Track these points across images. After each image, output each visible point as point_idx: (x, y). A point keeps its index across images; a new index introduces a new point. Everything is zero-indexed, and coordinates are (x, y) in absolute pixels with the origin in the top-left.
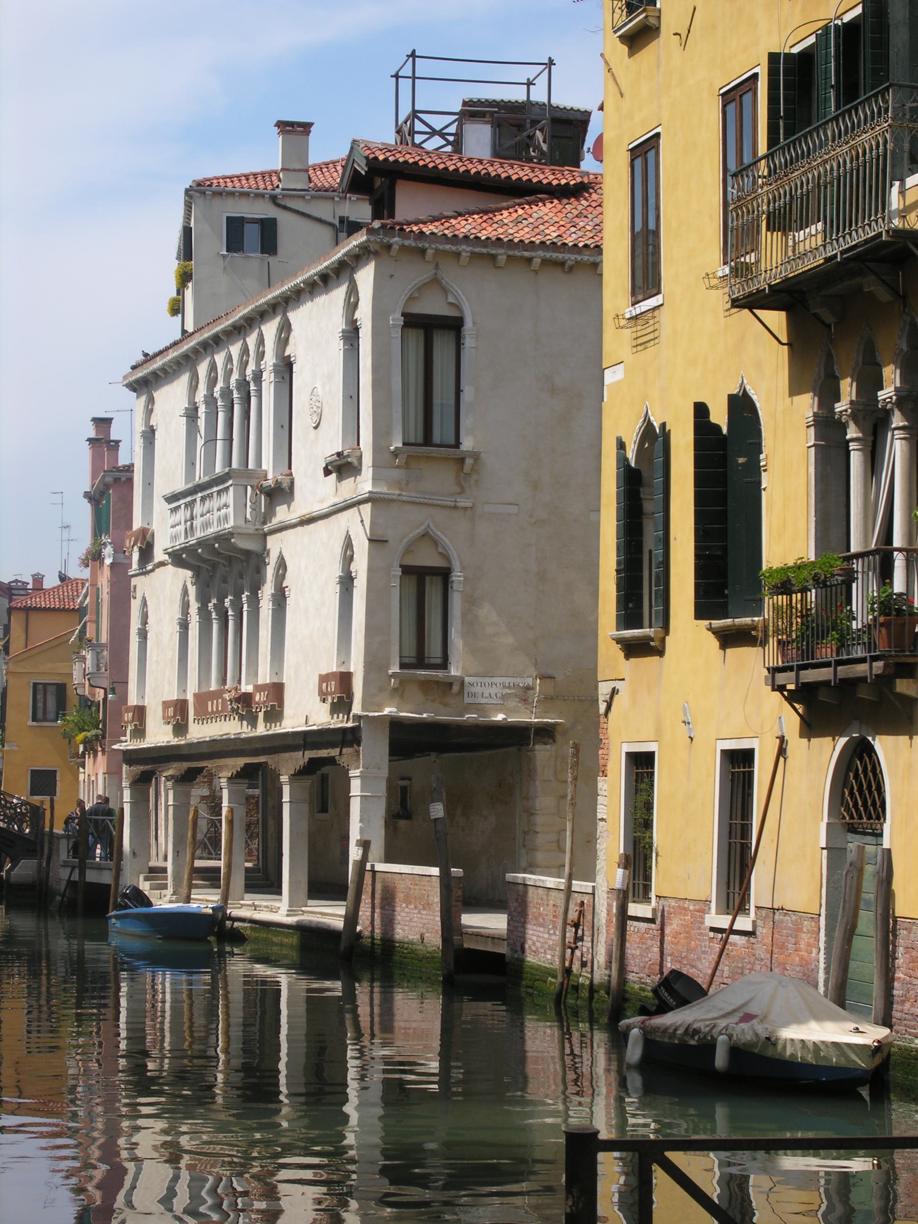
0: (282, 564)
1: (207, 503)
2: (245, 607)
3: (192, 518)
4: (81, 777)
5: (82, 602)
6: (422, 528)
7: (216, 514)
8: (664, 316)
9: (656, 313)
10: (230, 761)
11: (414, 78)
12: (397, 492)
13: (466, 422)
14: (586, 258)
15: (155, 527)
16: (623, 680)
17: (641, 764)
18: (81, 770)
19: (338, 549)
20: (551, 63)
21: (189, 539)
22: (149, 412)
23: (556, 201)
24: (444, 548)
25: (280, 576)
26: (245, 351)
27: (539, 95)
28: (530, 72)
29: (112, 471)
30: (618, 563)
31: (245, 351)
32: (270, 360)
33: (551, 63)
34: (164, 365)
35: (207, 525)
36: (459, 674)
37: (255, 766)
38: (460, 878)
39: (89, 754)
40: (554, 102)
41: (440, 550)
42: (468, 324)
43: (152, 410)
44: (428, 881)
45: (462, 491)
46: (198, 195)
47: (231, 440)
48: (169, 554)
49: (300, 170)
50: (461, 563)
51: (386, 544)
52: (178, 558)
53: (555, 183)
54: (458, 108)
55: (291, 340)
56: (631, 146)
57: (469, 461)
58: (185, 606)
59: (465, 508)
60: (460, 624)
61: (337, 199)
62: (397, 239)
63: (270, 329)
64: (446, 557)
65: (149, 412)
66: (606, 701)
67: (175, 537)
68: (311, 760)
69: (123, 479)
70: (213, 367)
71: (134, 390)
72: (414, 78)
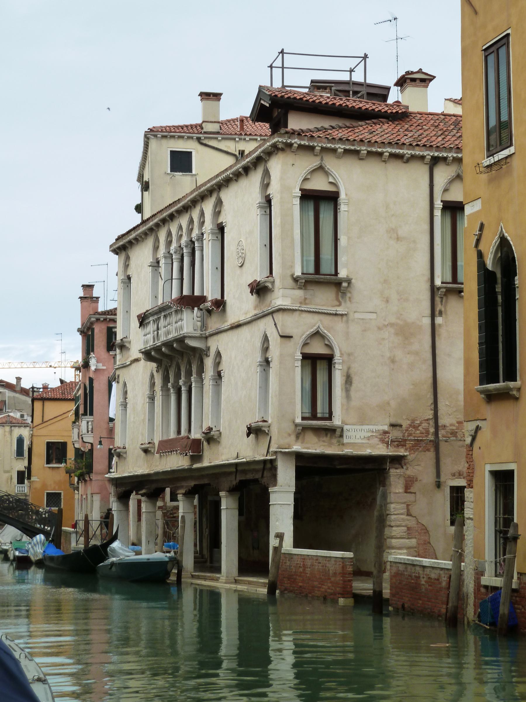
0: (218, 354)
1: (168, 319)
2: (193, 385)
3: (158, 329)
4: (76, 496)
5: (76, 394)
6: (315, 328)
7: (174, 325)
8: (515, 162)
9: (508, 160)
10: (184, 484)
11: (283, 68)
12: (299, 305)
13: (342, 259)
14: (417, 153)
15: (131, 338)
16: (486, 419)
17: (504, 480)
18: (76, 492)
19: (258, 344)
20: (365, 57)
21: (156, 342)
22: (126, 266)
23: (391, 123)
24: (329, 341)
25: (217, 364)
26: (191, 221)
27: (358, 77)
28: (351, 63)
29: (94, 314)
30: (480, 338)
31: (191, 221)
32: (208, 226)
33: (365, 57)
34: (136, 236)
35: (168, 333)
36: (340, 423)
37: (203, 487)
38: (351, 558)
39: (82, 482)
40: (368, 81)
41: (327, 343)
42: (343, 196)
43: (128, 265)
44: (328, 561)
45: (340, 305)
46: (152, 137)
47: (182, 279)
48: (142, 353)
49: (215, 122)
50: (340, 351)
51: (292, 339)
52: (148, 355)
53: (389, 111)
54: (308, 84)
55: (222, 210)
56: (484, 48)
57: (345, 284)
58: (152, 385)
59: (342, 315)
60: (340, 390)
61: (237, 139)
62: (296, 140)
63: (208, 206)
64: (329, 346)
65: (126, 266)
66: (471, 435)
67: (146, 342)
68: (241, 482)
69: (102, 319)
70: (169, 234)
71: (117, 254)
72: (283, 68)
